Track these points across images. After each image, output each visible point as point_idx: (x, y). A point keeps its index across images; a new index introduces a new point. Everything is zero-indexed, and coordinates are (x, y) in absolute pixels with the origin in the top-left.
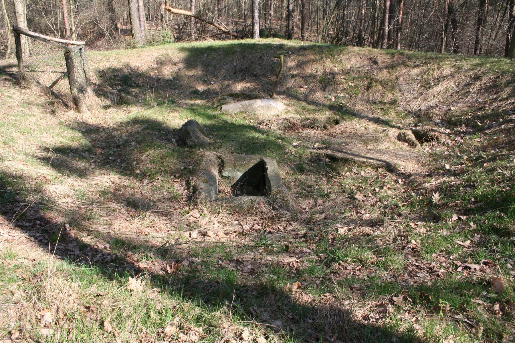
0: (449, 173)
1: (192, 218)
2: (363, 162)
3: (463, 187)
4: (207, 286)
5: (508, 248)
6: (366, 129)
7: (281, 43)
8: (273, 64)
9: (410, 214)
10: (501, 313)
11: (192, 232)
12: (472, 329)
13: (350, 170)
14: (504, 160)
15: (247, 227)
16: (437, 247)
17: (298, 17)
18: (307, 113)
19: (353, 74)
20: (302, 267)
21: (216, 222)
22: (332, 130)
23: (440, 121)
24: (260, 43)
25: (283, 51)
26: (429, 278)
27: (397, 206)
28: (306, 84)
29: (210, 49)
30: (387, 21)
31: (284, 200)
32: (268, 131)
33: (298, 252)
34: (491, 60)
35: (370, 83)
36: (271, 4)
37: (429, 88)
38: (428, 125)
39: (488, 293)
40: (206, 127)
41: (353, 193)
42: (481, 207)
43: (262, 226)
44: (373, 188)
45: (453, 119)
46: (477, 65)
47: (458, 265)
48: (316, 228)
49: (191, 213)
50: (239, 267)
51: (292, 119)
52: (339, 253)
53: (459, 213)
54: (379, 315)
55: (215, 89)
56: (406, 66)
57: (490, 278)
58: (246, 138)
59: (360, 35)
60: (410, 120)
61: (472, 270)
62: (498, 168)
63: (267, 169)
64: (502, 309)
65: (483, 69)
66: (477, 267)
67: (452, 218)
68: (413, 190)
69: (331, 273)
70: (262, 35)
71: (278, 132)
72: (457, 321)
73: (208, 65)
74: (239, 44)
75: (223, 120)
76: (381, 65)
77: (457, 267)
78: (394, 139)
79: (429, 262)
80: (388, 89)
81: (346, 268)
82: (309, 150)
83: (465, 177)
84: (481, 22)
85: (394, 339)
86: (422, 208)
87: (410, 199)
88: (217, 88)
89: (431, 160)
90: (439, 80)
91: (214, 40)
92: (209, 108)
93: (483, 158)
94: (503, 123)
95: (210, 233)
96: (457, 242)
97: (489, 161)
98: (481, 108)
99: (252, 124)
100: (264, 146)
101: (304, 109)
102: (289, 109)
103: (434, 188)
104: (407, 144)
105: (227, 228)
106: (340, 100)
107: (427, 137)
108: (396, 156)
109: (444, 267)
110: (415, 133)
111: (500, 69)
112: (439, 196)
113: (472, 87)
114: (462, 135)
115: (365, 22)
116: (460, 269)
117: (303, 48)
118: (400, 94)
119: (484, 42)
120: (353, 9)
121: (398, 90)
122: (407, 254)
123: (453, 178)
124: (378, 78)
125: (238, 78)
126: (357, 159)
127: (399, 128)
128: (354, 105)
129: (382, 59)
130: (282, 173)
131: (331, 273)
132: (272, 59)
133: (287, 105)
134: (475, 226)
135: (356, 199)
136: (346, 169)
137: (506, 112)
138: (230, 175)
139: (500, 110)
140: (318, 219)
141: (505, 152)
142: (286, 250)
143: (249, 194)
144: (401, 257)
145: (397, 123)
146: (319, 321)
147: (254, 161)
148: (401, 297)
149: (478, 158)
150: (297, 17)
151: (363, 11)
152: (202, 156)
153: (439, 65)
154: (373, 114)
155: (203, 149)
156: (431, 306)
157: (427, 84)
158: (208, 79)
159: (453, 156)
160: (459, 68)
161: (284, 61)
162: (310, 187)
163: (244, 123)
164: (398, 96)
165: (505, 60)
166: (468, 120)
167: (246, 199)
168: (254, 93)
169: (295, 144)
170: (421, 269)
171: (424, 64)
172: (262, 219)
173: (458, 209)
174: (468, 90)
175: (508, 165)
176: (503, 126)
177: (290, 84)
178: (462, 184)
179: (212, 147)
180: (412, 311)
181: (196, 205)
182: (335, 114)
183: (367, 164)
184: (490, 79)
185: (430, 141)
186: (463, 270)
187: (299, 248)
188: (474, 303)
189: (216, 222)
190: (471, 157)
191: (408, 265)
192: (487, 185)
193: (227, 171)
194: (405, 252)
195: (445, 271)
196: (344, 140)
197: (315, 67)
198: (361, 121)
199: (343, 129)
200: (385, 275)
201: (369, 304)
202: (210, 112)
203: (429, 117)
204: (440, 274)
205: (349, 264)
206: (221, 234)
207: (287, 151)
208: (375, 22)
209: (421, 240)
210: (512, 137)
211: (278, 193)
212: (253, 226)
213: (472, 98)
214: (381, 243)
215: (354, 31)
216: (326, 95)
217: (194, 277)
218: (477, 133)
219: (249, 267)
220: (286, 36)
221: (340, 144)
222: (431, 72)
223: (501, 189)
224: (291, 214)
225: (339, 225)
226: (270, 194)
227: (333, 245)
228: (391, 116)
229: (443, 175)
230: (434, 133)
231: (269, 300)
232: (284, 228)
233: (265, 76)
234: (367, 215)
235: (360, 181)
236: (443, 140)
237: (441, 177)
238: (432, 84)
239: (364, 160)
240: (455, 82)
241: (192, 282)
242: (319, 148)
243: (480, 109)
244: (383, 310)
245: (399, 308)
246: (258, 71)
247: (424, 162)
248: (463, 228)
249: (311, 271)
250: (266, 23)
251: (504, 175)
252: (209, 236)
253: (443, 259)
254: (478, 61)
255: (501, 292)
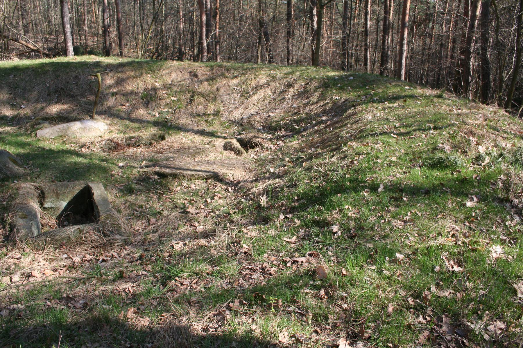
0: (273, 175)
1: (12, 260)
2: (192, 176)
3: (287, 188)
4: (31, 333)
5: (328, 237)
6: (193, 142)
7: (97, 60)
8: (91, 83)
9: (241, 220)
10: (326, 297)
11: (12, 275)
12: (303, 317)
13: (180, 185)
14: (319, 158)
15: (77, 259)
16: (267, 247)
17: (115, 33)
18: (132, 132)
19: (175, 89)
20: (139, 290)
21: (41, 260)
22: (158, 147)
23: (261, 127)
24: (75, 61)
25: (101, 69)
26: (262, 278)
27: (229, 214)
28: (128, 101)
29: (15, 69)
30: (204, 35)
31: (114, 224)
32: (91, 154)
33: (134, 276)
34: (300, 68)
35: (192, 96)
36: (84, 20)
37: (249, 97)
38: (251, 132)
39: (314, 281)
40: (20, 157)
41: (185, 207)
42: (304, 203)
43: (94, 255)
44: (204, 200)
45: (273, 125)
46: (289, 74)
47: (288, 261)
48: (151, 248)
49: (10, 255)
50: (70, 305)
51: (116, 139)
52: (174, 270)
53: (285, 213)
54: (217, 324)
55: (27, 114)
56: (226, 77)
57: (315, 267)
58: (68, 164)
59: (180, 49)
60: (234, 129)
61: (300, 263)
62: (314, 166)
63: (93, 194)
64: (326, 293)
65: (294, 77)
66: (304, 259)
67: (279, 218)
68: (243, 196)
69: (168, 292)
70: (77, 52)
71: (103, 154)
72: (289, 313)
73: (16, 87)
74: (50, 63)
75: (39, 147)
76: (201, 77)
77: (286, 262)
78: (220, 149)
79: (261, 263)
80: (211, 101)
81: (182, 284)
82: (136, 170)
83: (288, 177)
84: (289, 34)
85: (234, 343)
86: (252, 213)
87: (240, 205)
88: (29, 112)
89: (257, 165)
90: (257, 88)
91: (21, 59)
92: (22, 135)
93: (302, 158)
94: (316, 125)
95: (35, 273)
96: (285, 239)
97: (307, 160)
98: (297, 113)
99: (73, 149)
100: (89, 170)
101: (128, 128)
102: (112, 129)
103: (262, 192)
104: (233, 152)
105: (54, 264)
106: (164, 115)
107: (251, 144)
108: (223, 165)
109: (275, 265)
110: (240, 141)
111: (308, 77)
112: (266, 199)
113: (287, 93)
114: (283, 139)
115: (184, 36)
116: (289, 264)
117: (121, 65)
118: (222, 105)
119: (294, 53)
120: (171, 23)
121: (220, 101)
122: (240, 259)
123: (277, 180)
124: (200, 91)
125: (53, 100)
126: (185, 172)
127: (225, 138)
128: (178, 119)
129: (201, 72)
130: (111, 197)
131: (168, 291)
132: (90, 77)
133: (110, 125)
134: (299, 222)
135: (189, 212)
136: (176, 184)
137: (317, 115)
138: (53, 206)
139: (313, 113)
140: (153, 239)
141: (319, 151)
142: (121, 276)
143: (75, 223)
144: (235, 263)
145: (222, 133)
146: (158, 343)
147: (77, 188)
148: (237, 302)
149: (298, 159)
150: (113, 33)
151: (182, 26)
152: (18, 189)
153: (255, 75)
154: (198, 126)
155: (18, 181)
156: (265, 304)
157: (247, 94)
158: (17, 103)
159: (276, 159)
160: (273, 77)
161: (102, 80)
162: (141, 207)
163: (65, 148)
164: (221, 107)
165: (312, 68)
166: (286, 124)
167: (72, 230)
168: (72, 115)
169: (121, 164)
170: (254, 271)
171: (241, 74)
172: (93, 247)
173: (284, 208)
174: (283, 97)
175: (323, 163)
176: (316, 128)
177: (111, 102)
178: (285, 184)
179: (29, 178)
180: (249, 313)
181: (15, 244)
182: (160, 130)
183: (196, 176)
184: (301, 85)
185: (254, 147)
186: (292, 264)
187: (135, 272)
188: (303, 293)
189: (41, 260)
190: (292, 158)
191: (242, 270)
192: (307, 183)
193: (49, 202)
194: (238, 257)
195: (276, 269)
196: (171, 155)
197: (136, 84)
198: (187, 134)
199: (169, 144)
200: (222, 284)
201: (207, 315)
202: (23, 139)
203: (251, 124)
204: (272, 272)
205: (185, 279)
206: (49, 272)
207: (113, 172)
208: (193, 36)
209: (252, 243)
210: (324, 136)
211: (107, 218)
212: (84, 257)
213: (288, 104)
214: (216, 253)
215: (174, 45)
216: (149, 112)
217: (15, 327)
218: (295, 136)
219: (81, 302)
220: (104, 53)
221: (167, 160)
222: (249, 82)
223: (318, 185)
224: (124, 238)
225: (174, 242)
226: (99, 220)
227: (169, 263)
228: (216, 127)
229: (269, 178)
230: (257, 140)
231: (104, 332)
232: (118, 254)
233: (83, 96)
234: (201, 227)
235: (191, 194)
236: (266, 145)
237: (267, 180)
238: (251, 93)
239: (193, 173)
240: (271, 90)
241: (12, 333)
242: (146, 167)
243: (295, 114)
244: (221, 318)
245: (236, 313)
246: (75, 91)
247: (250, 168)
248: (290, 226)
249: (148, 292)
250: (80, 40)
251: (320, 171)
252: (34, 276)
253: (273, 258)
254: (289, 70)
255: (325, 278)
